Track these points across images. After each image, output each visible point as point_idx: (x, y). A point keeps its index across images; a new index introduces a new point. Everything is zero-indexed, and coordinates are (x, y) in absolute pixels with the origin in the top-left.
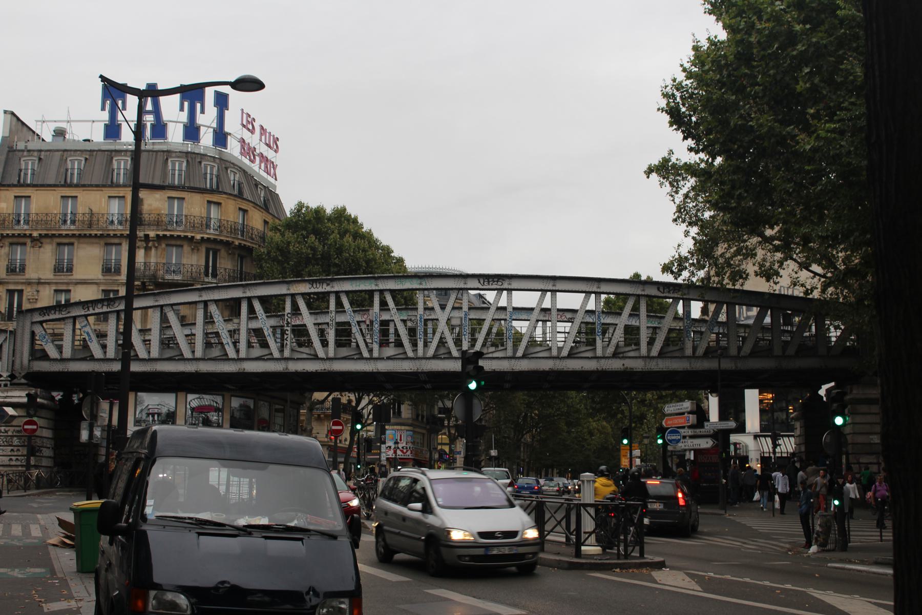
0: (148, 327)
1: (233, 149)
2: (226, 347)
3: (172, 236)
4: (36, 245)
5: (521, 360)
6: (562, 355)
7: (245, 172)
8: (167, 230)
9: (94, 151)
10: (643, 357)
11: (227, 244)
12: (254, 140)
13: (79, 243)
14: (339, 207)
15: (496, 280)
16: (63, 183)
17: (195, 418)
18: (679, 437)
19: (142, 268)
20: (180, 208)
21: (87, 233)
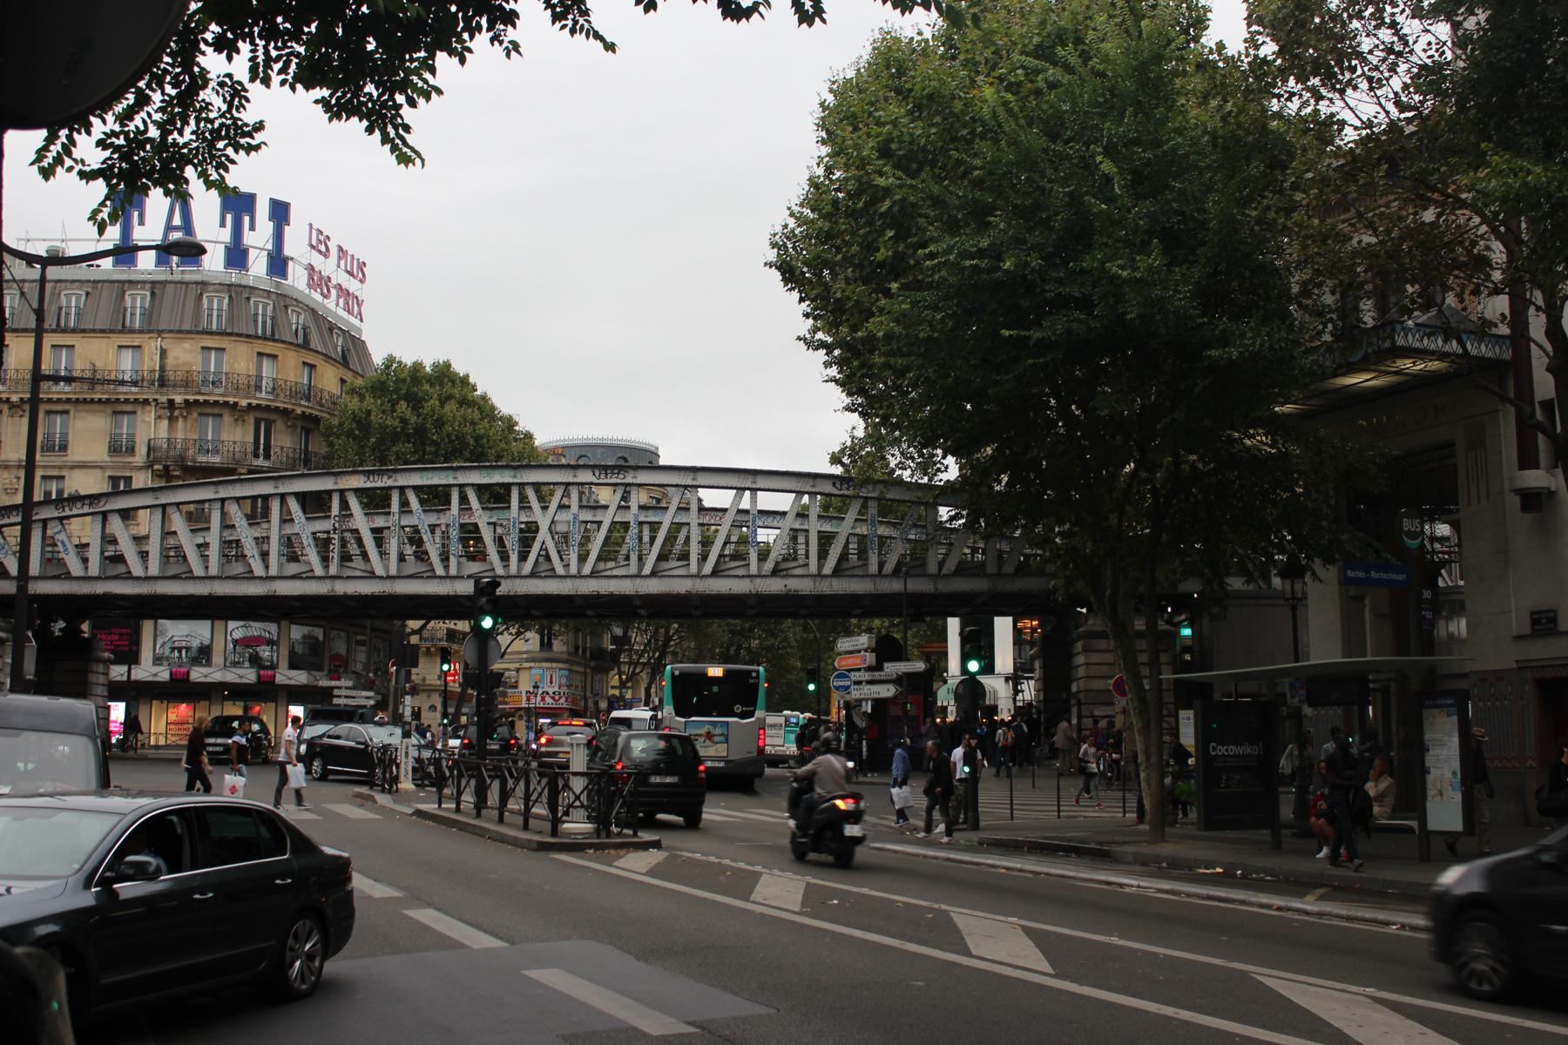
0: (173, 529)
1: (297, 279)
2: (251, 561)
3: (206, 402)
4: (16, 413)
5: (648, 580)
6: (703, 574)
7: (314, 312)
8: (199, 393)
9: (99, 281)
10: (812, 576)
11: (286, 413)
12: (328, 266)
13: (76, 411)
14: (441, 362)
15: (616, 471)
16: (54, 327)
17: (239, 653)
18: (849, 683)
19: (165, 446)
20: (219, 363)
21: (88, 397)
